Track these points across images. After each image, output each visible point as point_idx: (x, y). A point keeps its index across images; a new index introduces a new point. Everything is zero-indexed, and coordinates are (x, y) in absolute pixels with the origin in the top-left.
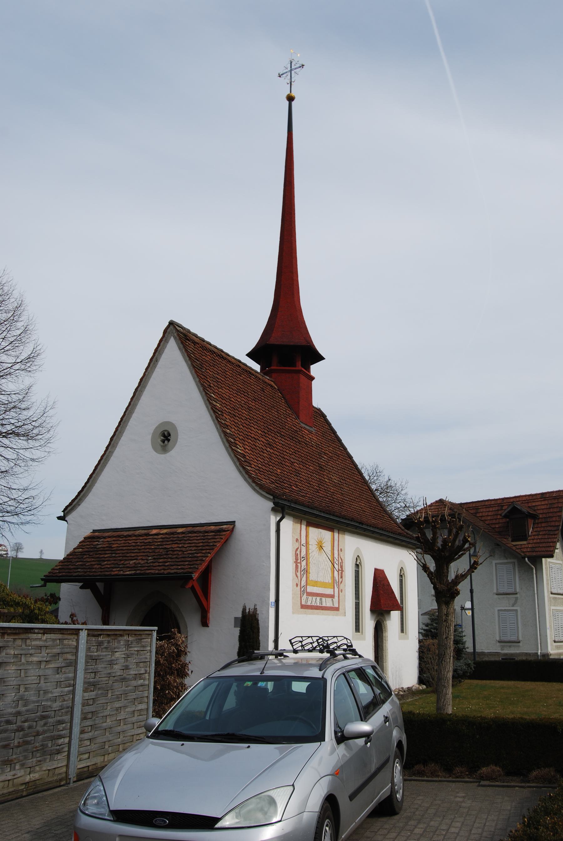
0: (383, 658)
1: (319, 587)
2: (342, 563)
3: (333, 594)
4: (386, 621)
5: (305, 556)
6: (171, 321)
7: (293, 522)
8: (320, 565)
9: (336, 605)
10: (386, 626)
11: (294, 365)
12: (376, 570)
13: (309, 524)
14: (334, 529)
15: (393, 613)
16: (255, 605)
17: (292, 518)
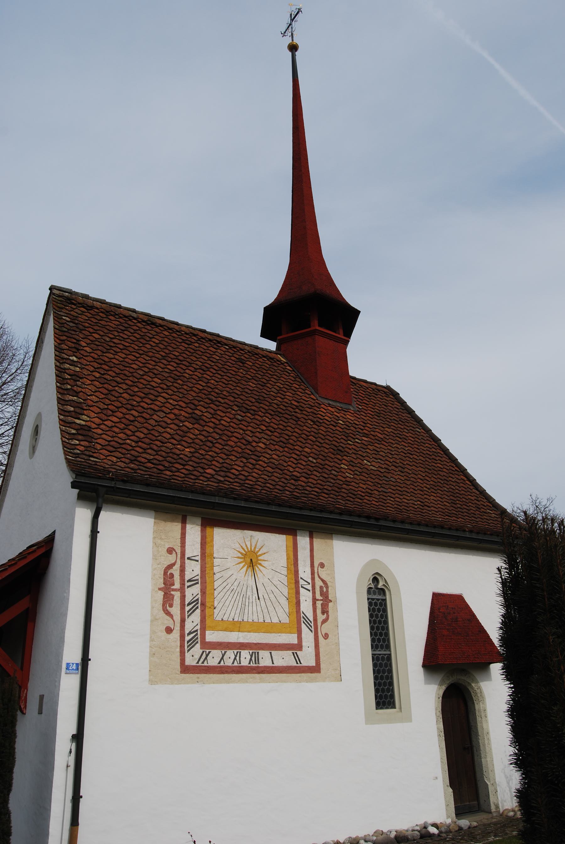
0: (480, 750)
1: (249, 632)
2: (327, 587)
5: (199, 577)
6: (52, 286)
7: (155, 519)
10: (478, 691)
15: (492, 666)
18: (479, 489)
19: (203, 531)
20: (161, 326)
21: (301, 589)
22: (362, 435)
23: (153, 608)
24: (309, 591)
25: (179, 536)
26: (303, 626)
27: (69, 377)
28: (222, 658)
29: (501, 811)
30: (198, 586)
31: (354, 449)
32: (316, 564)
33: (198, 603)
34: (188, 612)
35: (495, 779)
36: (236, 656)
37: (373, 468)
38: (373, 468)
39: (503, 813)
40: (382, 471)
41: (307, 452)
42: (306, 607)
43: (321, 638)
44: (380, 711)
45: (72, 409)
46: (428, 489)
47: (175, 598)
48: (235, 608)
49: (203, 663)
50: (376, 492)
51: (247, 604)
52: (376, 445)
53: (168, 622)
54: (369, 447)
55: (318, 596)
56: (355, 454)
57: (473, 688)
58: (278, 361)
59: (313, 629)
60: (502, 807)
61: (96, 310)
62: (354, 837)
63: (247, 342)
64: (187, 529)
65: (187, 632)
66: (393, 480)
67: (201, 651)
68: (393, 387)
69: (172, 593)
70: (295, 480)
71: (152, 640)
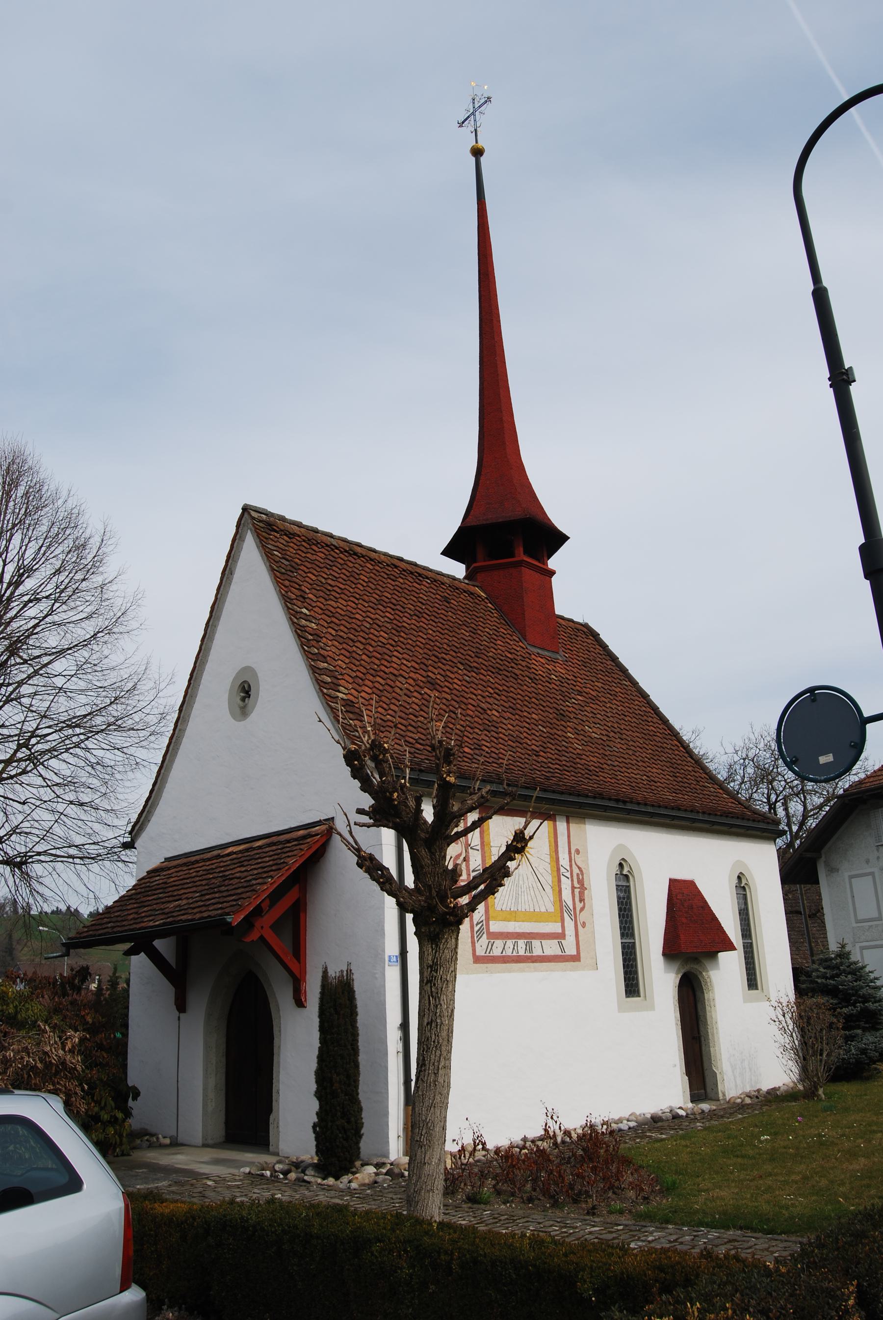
0: (708, 1039)
2: (582, 875)
4: (708, 971)
8: (521, 882)
9: (571, 950)
10: (708, 980)
11: (512, 555)
12: (674, 884)
14: (554, 815)
16: (349, 964)
18: (694, 757)
20: (363, 556)
21: (562, 876)
26: (565, 914)
28: (504, 948)
29: (727, 1100)
32: (573, 851)
37: (596, 736)
38: (596, 736)
39: (729, 1100)
40: (605, 738)
43: (580, 927)
44: (629, 999)
45: (329, 680)
48: (511, 897)
50: (605, 766)
52: (591, 705)
54: (586, 708)
55: (576, 885)
57: (703, 977)
58: (479, 596)
61: (298, 538)
63: (445, 572)
65: (475, 923)
67: (488, 941)
70: (536, 756)
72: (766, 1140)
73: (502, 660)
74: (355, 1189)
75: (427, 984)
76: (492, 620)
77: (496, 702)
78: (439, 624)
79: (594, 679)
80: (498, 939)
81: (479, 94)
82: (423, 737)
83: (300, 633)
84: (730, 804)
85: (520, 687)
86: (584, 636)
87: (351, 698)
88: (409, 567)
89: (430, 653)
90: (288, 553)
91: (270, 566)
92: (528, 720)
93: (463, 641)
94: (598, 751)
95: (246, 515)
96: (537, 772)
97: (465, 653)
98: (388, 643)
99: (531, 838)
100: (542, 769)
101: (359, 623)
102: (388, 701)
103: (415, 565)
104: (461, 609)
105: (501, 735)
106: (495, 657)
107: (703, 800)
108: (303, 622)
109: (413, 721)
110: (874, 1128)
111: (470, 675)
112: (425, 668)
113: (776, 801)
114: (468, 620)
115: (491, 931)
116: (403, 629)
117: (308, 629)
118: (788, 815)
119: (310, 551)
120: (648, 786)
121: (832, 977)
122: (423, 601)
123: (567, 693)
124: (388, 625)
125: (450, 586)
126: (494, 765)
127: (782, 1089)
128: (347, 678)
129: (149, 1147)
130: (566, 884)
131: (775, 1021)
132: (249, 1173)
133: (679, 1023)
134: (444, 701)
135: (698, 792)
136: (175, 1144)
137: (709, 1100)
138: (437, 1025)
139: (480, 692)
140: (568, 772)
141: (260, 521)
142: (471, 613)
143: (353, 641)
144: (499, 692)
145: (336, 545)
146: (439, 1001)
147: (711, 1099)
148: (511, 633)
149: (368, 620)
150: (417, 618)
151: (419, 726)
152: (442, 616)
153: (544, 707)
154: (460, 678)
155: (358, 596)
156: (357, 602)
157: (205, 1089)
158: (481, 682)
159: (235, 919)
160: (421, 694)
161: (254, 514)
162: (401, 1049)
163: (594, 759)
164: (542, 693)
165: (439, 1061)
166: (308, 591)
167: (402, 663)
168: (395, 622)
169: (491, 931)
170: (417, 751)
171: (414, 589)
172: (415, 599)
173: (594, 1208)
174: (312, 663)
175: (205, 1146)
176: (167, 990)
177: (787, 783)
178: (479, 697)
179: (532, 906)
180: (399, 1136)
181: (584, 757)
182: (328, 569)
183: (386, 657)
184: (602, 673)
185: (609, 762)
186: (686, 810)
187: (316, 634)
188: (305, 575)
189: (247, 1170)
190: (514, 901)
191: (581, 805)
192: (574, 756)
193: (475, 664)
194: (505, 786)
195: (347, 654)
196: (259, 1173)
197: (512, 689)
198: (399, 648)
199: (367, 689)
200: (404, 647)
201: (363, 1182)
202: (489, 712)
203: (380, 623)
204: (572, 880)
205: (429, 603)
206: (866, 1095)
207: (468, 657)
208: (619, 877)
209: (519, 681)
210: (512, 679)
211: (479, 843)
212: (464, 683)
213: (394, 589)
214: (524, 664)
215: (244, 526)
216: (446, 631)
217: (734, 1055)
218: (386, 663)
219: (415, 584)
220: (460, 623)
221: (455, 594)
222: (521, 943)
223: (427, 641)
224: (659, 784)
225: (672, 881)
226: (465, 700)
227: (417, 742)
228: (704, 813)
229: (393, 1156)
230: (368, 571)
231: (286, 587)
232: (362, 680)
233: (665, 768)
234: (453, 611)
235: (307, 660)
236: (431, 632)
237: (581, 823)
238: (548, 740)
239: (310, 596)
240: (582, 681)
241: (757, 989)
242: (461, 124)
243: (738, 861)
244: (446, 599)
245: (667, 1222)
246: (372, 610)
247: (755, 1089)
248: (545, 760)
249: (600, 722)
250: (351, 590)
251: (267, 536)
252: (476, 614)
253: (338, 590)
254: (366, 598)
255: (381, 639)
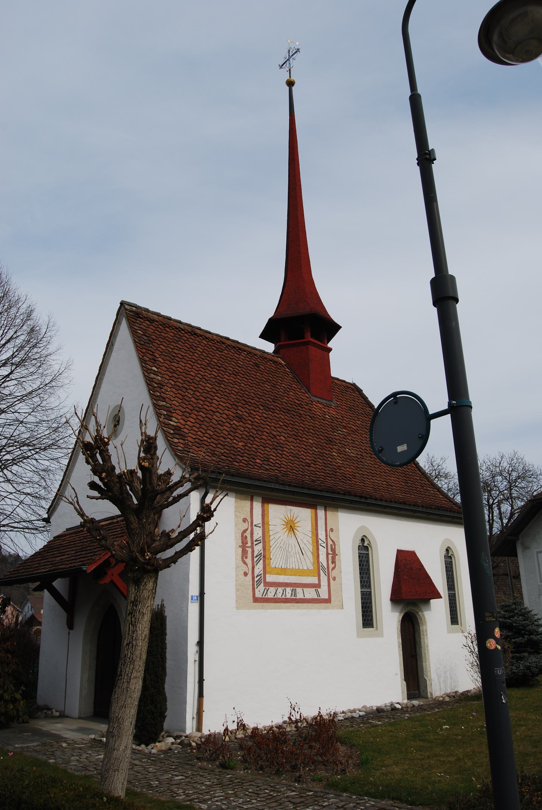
1: (290, 575)
2: (335, 545)
3: (317, 583)
4: (422, 612)
5: (261, 538)
8: (290, 549)
9: (324, 595)
10: (423, 618)
12: (400, 554)
13: (266, 500)
16: (163, 601)
17: (234, 494)
19: (263, 506)
20: (201, 336)
21: (320, 546)
22: (342, 427)
23: (236, 559)
24: (324, 547)
25: (249, 510)
26: (321, 571)
27: (157, 386)
28: (276, 593)
29: (434, 698)
30: (261, 544)
31: (339, 440)
33: (261, 556)
34: (256, 562)
35: (431, 677)
36: (283, 591)
37: (353, 455)
38: (353, 455)
40: (359, 457)
41: (311, 443)
42: (323, 559)
46: (389, 471)
47: (249, 552)
48: (282, 559)
49: (265, 596)
50: (357, 474)
51: (289, 557)
52: (352, 435)
53: (245, 569)
54: (348, 437)
55: (330, 552)
56: (340, 443)
57: (419, 615)
58: (280, 364)
59: (327, 574)
60: (435, 695)
61: (156, 323)
62: (352, 709)
64: (254, 505)
65: (256, 575)
66: (367, 464)
67: (264, 588)
68: (358, 384)
69: (247, 549)
70: (308, 466)
71: (237, 581)
72: (446, 728)
73: (291, 405)
74: (154, 754)
75: (129, 615)
76: (288, 379)
77: (284, 431)
78: (249, 380)
79: (356, 419)
80: (271, 586)
81: (293, 48)
82: (227, 452)
83: (149, 382)
84: (443, 502)
85: (302, 422)
86: (352, 392)
87: (179, 425)
88: (233, 344)
89: (240, 398)
90: (148, 332)
91: (134, 339)
92: (305, 443)
93: (265, 392)
94: (354, 465)
95: (122, 308)
96: (307, 477)
97: (265, 399)
98: (211, 391)
99: (215, 510)
100: (311, 475)
101: (192, 378)
102: (206, 428)
103: (237, 342)
104: (266, 371)
105: (285, 453)
106: (287, 402)
107: (425, 498)
108: (152, 376)
109: (222, 441)
110: (522, 722)
111: (267, 413)
112: (235, 407)
113: (493, 504)
114: (270, 378)
115: (267, 581)
116: (223, 382)
117: (154, 380)
118: (500, 513)
119: (164, 331)
120: (386, 488)
121: (509, 618)
122: (240, 366)
123: (335, 427)
124: (213, 380)
125: (260, 357)
126: (276, 471)
127: (472, 692)
128: (178, 412)
129: (45, 717)
130: (323, 552)
131: (466, 646)
132: (94, 739)
133: (401, 646)
134: (247, 429)
135: (422, 493)
136: (63, 716)
137: (421, 697)
138: (133, 646)
139: (273, 424)
140: (330, 477)
141: (131, 311)
142: (273, 374)
143: (186, 389)
144: (287, 425)
145: (183, 328)
146: (136, 628)
147: (423, 697)
148: (300, 388)
149: (199, 376)
150: (234, 376)
151: (226, 445)
152: (252, 375)
153: (318, 435)
154: (260, 415)
155: (194, 361)
156: (192, 364)
157: (82, 681)
158: (275, 418)
159: (89, 569)
160: (230, 424)
161: (127, 307)
162: (197, 658)
163: (350, 470)
164: (318, 426)
165: (131, 673)
166: (158, 356)
167: (220, 404)
168: (218, 378)
169: (267, 581)
170: (222, 461)
171: (234, 357)
172: (234, 364)
173: (300, 777)
174: (155, 402)
175: (80, 718)
176: (63, 615)
177: (500, 492)
178: (272, 428)
179: (297, 565)
180: (193, 718)
181: (343, 468)
182: (175, 343)
183: (209, 400)
184: (362, 415)
185: (360, 472)
186: (410, 505)
187: (160, 384)
188: (158, 346)
189: (93, 736)
190: (284, 561)
191: (334, 499)
192: (336, 468)
193: (272, 407)
194: (200, 472)
195: (181, 397)
196: (99, 739)
197: (296, 423)
198: (218, 395)
199: (192, 420)
200: (222, 394)
201: (161, 749)
202: (278, 437)
203: (207, 378)
204: (327, 549)
205: (244, 366)
206: (526, 698)
207: (267, 402)
208: (362, 548)
209: (302, 418)
210: (297, 417)
211: (261, 522)
212: (263, 418)
213: (221, 357)
214: (307, 407)
215: (121, 314)
216: (254, 385)
217: (439, 668)
218: (208, 404)
219: (236, 355)
220: (265, 380)
221: (263, 362)
222: (289, 590)
223: (239, 390)
224: (394, 487)
225: (398, 551)
226: (262, 429)
227: (222, 455)
228: (423, 507)
229: (188, 731)
230: (204, 345)
231: (143, 353)
232: (189, 414)
233: (400, 477)
234: (261, 372)
235: (152, 400)
236: (243, 385)
237: (335, 511)
238: (318, 456)
239: (160, 359)
240: (347, 420)
241: (458, 624)
242: (281, 67)
243: (447, 539)
244: (257, 365)
245: (345, 791)
246: (203, 370)
247: (454, 691)
248: (314, 469)
249: (357, 446)
250: (190, 357)
251: (134, 320)
252: (277, 375)
253: (180, 356)
254: (199, 362)
255: (207, 388)
